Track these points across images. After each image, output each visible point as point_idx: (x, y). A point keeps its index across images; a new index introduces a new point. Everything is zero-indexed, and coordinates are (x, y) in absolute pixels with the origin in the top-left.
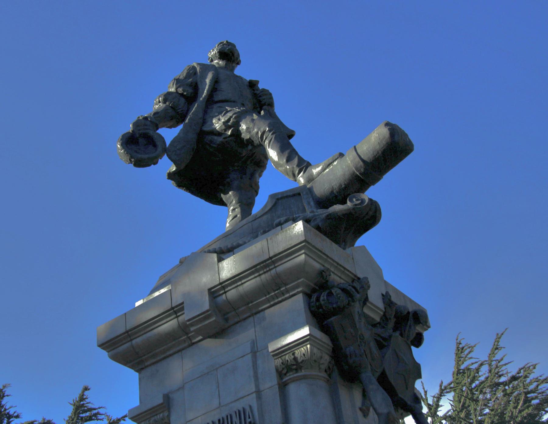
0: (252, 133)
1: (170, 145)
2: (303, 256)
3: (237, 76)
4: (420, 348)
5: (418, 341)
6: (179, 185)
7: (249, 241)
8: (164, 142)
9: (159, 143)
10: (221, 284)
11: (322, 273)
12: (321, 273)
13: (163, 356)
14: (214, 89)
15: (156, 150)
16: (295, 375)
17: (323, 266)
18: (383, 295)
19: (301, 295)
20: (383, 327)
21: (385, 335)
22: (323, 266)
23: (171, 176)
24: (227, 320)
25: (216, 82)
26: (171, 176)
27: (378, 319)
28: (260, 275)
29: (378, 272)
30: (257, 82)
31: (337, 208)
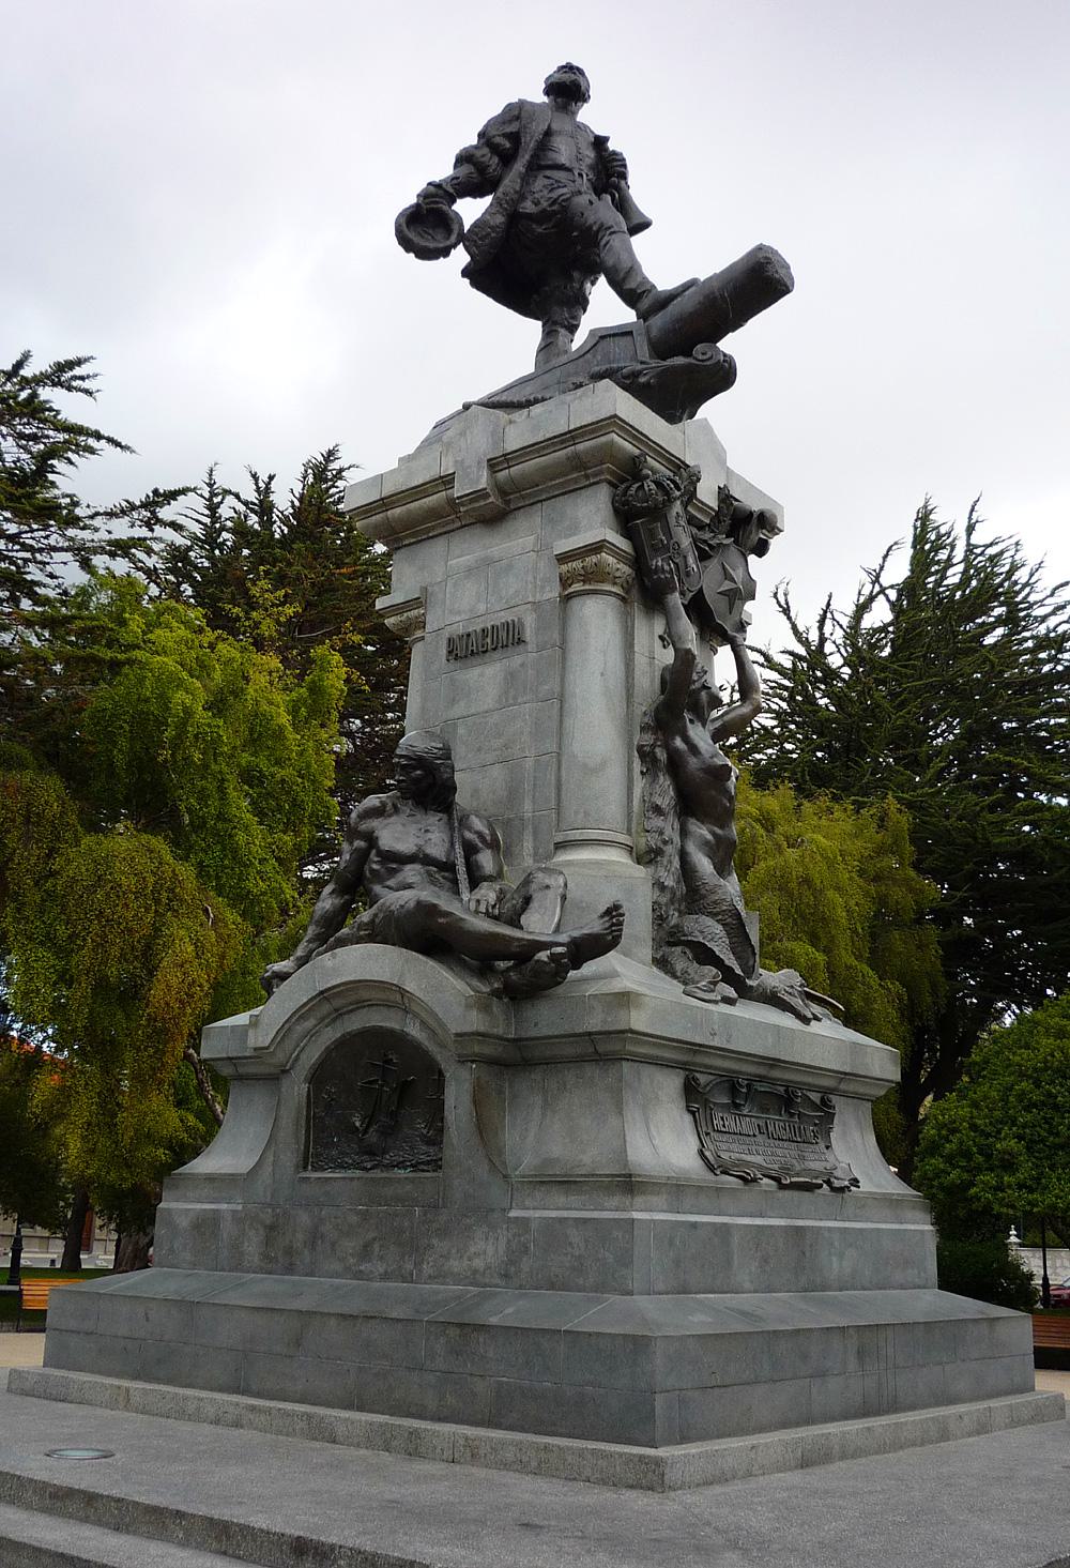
1: (469, 230)
3: (469, 253)
4: (764, 558)
5: (761, 549)
8: (462, 225)
9: (456, 227)
10: (504, 455)
13: (444, 530)
15: (448, 238)
16: (582, 588)
18: (719, 488)
20: (713, 531)
24: (508, 502)
29: (721, 459)
30: (606, 139)
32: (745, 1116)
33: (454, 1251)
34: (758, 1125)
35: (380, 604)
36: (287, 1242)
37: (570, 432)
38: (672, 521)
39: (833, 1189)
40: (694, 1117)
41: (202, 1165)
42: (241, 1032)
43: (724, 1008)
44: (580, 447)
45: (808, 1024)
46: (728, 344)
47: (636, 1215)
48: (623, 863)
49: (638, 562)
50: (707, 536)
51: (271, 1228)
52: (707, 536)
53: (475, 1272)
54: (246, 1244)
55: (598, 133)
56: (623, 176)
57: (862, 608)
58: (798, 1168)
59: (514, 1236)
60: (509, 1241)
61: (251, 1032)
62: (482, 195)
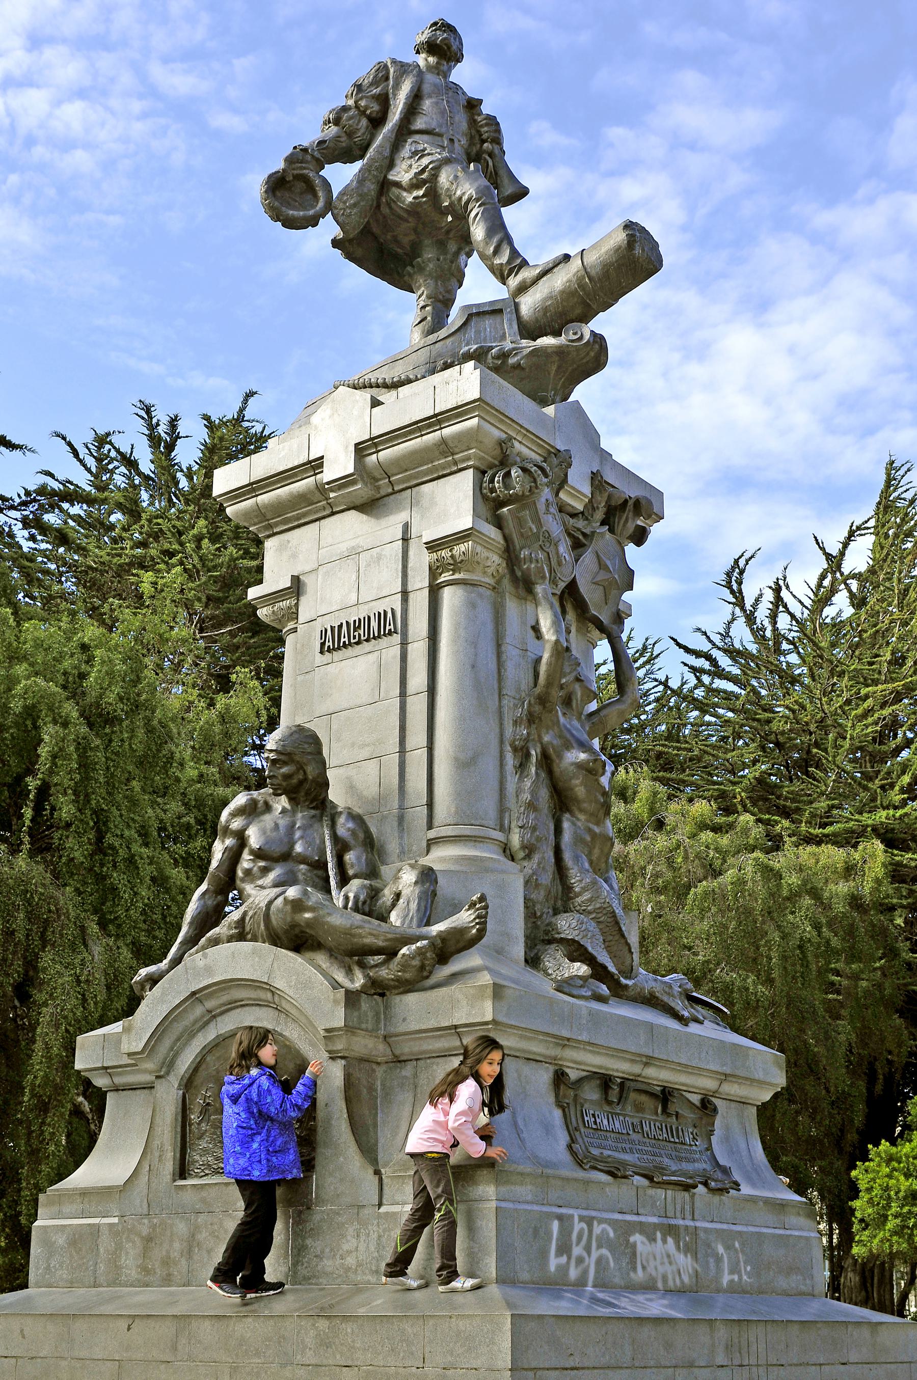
0: (453, 198)
2: (476, 420)
6: (350, 257)
7: (424, 377)
11: (501, 444)
12: (501, 443)
13: (296, 523)
14: (412, 109)
17: (506, 433)
19: (471, 470)
20: (587, 519)
21: (587, 531)
22: (506, 433)
23: (336, 243)
25: (416, 97)
26: (336, 243)
27: (580, 507)
28: (422, 435)
30: (480, 101)
31: (547, 341)
32: (618, 1114)
33: (327, 1250)
34: (633, 1124)
35: (253, 593)
36: (164, 1253)
37: (435, 415)
38: (541, 507)
39: (711, 1190)
40: (564, 1111)
41: (81, 1177)
42: (117, 1039)
43: (596, 1006)
44: (447, 432)
45: (687, 1025)
46: (601, 323)
47: (204, 887)
48: (495, 860)
49: (510, 554)
50: (580, 524)
51: (149, 1239)
52: (580, 524)
53: (348, 1269)
54: (124, 1258)
55: (470, 94)
56: (497, 140)
57: (823, 599)
58: (674, 1168)
59: (384, 1231)
60: (380, 1237)
61: (124, 1039)
62: (352, 161)
